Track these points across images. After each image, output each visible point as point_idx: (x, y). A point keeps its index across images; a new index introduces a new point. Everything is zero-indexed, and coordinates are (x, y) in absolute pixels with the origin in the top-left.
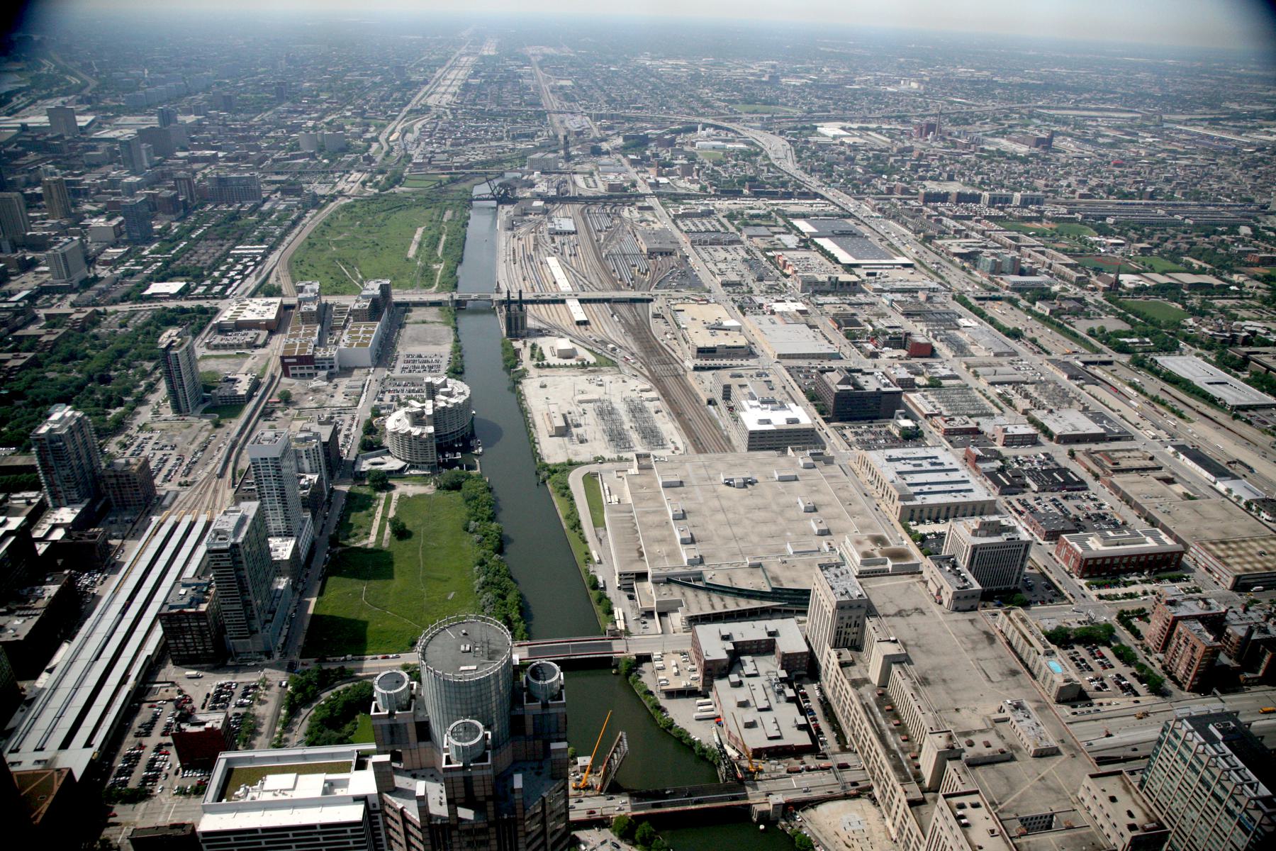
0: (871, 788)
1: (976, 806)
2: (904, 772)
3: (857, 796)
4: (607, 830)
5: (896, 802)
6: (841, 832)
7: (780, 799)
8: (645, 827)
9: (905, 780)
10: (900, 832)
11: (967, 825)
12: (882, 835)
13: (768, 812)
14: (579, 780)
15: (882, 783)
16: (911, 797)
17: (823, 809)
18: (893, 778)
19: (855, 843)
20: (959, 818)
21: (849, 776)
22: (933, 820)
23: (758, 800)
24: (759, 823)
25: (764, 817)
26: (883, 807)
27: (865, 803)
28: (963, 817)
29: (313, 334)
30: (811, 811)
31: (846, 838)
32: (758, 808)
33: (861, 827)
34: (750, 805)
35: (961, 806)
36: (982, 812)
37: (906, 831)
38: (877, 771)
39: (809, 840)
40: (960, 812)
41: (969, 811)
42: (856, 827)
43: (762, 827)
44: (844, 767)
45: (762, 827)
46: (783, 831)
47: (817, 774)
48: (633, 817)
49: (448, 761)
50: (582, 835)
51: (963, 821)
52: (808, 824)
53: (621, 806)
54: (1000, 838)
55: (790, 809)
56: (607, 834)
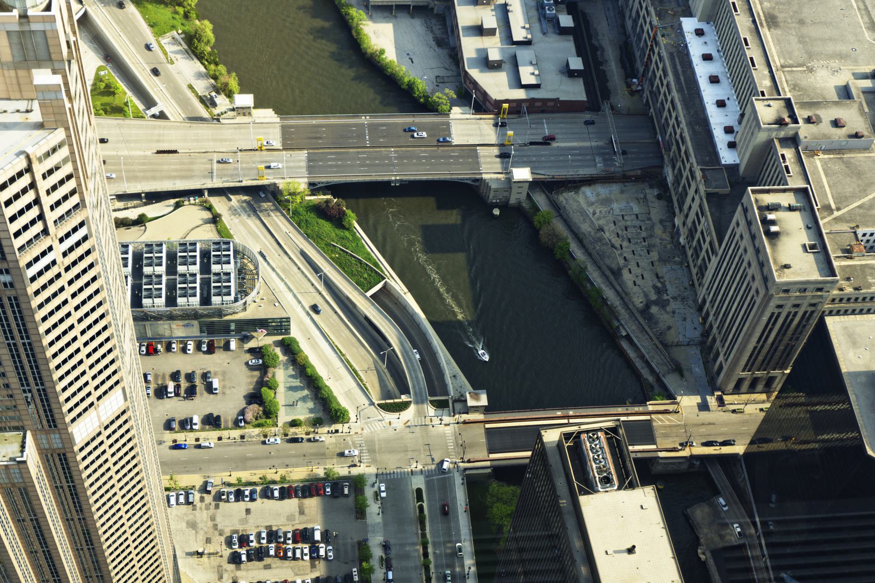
5: (691, 192)
11: (776, 235)
18: (693, 159)
28: (773, 222)
37: (698, 235)
51: (774, 229)
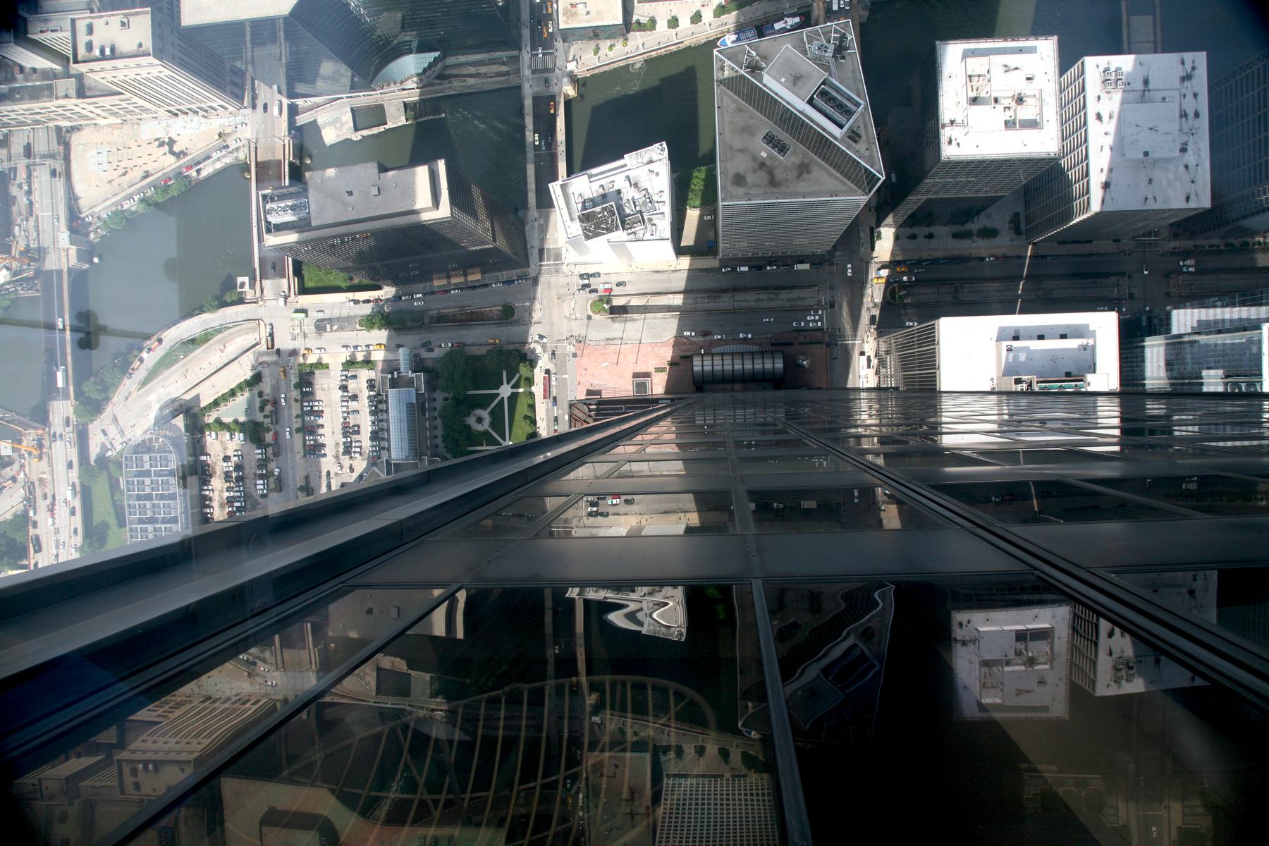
0: (58, 129)
1: (90, 29)
2: (41, 88)
3: (67, 146)
4: (91, 426)
5: (77, 109)
6: (108, 176)
7: (64, 236)
8: (90, 388)
9: (50, 92)
10: (115, 114)
11: (113, 49)
12: (117, 132)
13: (78, 251)
14: (30, 454)
15: (52, 115)
16: (73, 92)
17: (79, 189)
18: (48, 104)
19: (122, 165)
20: (103, 58)
21: (41, 146)
22: (104, 81)
23: (64, 260)
24: (91, 262)
25: (81, 256)
26: (83, 122)
27: (75, 139)
28: (102, 51)
29: (444, 459)
30: (82, 203)
31: (116, 174)
32: (73, 261)
33: (105, 153)
34: (70, 271)
35: (89, 46)
36: (98, 24)
37: (114, 109)
38: (38, 117)
39: (115, 213)
40: (97, 53)
41: (97, 40)
42: (104, 158)
43: (96, 260)
44: (28, 152)
45: (96, 260)
46: (102, 237)
47: (36, 185)
48: (76, 398)
49: (701, 751)
50: (94, 451)
52: (96, 210)
53: (62, 410)
54: (131, 19)
55: (76, 224)
56: (94, 428)
